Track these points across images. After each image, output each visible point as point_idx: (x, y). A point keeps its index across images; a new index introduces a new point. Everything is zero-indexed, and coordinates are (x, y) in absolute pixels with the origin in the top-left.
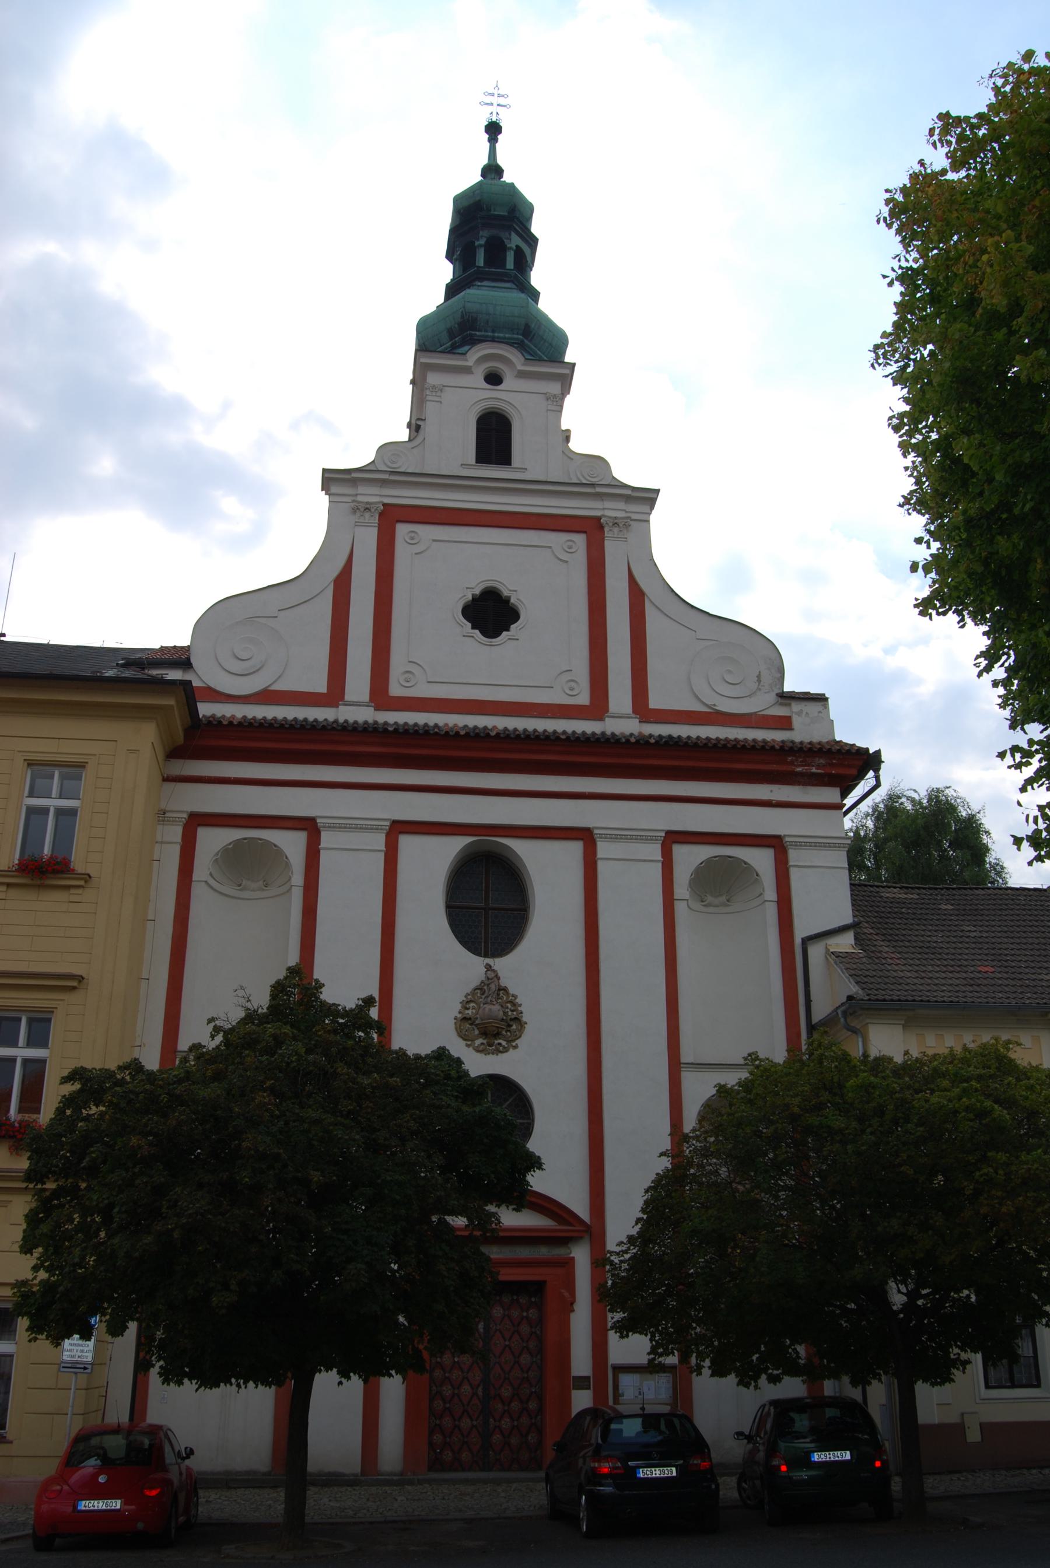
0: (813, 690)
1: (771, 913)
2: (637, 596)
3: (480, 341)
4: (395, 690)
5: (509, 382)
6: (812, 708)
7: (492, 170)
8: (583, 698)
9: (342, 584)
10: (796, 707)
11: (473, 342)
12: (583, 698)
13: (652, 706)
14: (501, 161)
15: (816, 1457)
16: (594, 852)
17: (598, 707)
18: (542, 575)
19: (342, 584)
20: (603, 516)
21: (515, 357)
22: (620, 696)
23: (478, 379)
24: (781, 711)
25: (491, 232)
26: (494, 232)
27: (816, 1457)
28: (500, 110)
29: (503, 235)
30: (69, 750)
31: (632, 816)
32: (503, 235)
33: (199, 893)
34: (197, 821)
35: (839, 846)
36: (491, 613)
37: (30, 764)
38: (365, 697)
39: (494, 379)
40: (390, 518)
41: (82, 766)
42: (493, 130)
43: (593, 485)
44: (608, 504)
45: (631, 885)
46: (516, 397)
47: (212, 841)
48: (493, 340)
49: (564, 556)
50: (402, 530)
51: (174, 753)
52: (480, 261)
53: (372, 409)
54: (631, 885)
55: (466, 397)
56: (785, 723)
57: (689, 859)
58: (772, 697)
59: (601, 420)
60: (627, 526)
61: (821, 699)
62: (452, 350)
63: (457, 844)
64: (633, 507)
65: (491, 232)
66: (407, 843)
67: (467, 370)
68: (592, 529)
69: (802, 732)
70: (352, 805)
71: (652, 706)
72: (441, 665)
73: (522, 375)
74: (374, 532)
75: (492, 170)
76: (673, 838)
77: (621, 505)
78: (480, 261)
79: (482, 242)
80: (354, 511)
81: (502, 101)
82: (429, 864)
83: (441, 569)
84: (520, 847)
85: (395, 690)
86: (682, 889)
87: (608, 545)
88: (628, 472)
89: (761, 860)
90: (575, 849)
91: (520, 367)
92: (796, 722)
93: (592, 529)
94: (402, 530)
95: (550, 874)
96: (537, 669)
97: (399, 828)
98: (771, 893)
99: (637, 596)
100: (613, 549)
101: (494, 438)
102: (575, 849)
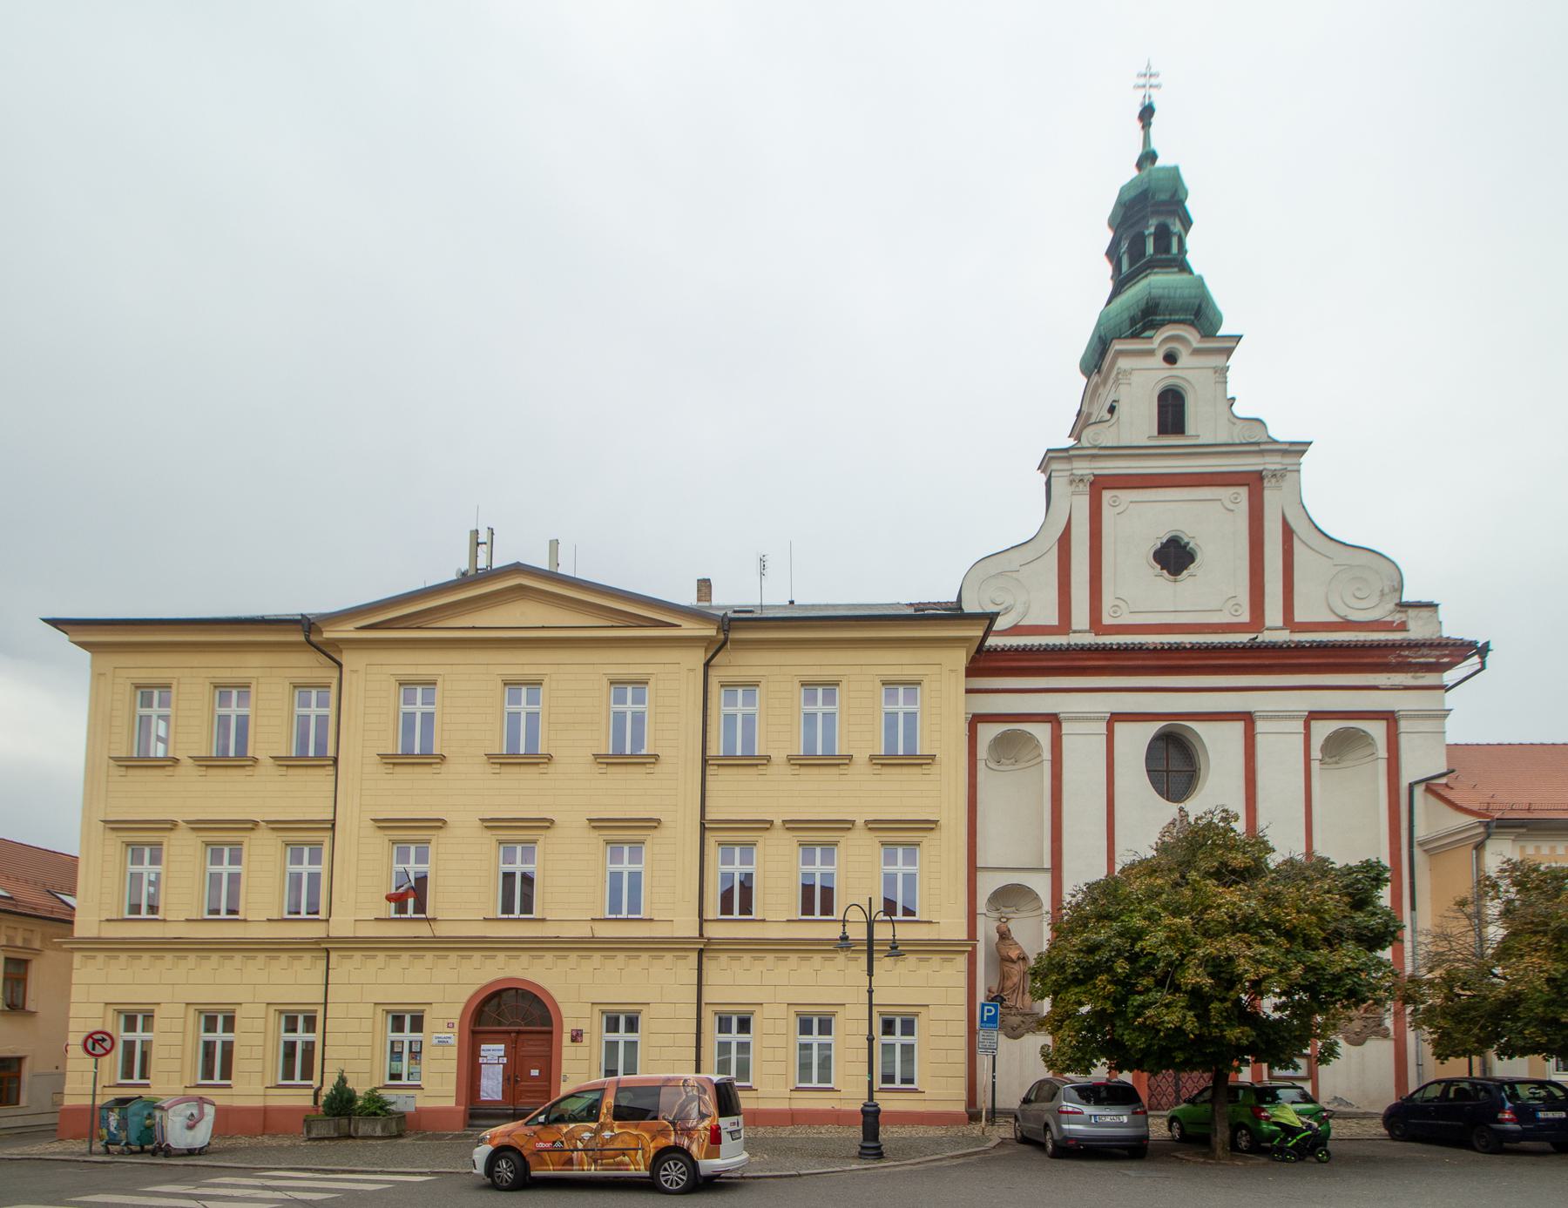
0: (1425, 599)
1: (1382, 766)
2: (1288, 533)
3: (1162, 324)
4: (1107, 620)
5: (1185, 359)
6: (1425, 613)
7: (1148, 158)
8: (1245, 617)
9: (1065, 542)
10: (1412, 612)
11: (1156, 326)
12: (1245, 617)
13: (1297, 619)
14: (1155, 145)
15: (1541, 1115)
16: (1253, 729)
17: (1065, 625)
18: (1214, 523)
19: (1065, 542)
20: (1257, 472)
21: (1192, 335)
22: (1273, 613)
23: (1158, 361)
24: (1398, 618)
25: (1149, 223)
26: (1162, 219)
27: (1541, 1115)
28: (1153, 92)
29: (1169, 221)
30: (827, 673)
31: (1281, 703)
32: (1169, 221)
33: (981, 766)
34: (976, 720)
35: (1297, 717)
36: (1174, 556)
37: (884, 683)
38: (1280, 623)
39: (1171, 358)
40: (1099, 485)
41: (837, 684)
42: (1147, 114)
43: (1258, 444)
44: (1268, 459)
45: (1281, 749)
46: (1191, 372)
47: (988, 733)
48: (1170, 322)
49: (1231, 506)
50: (1107, 495)
51: (971, 672)
52: (1150, 249)
53: (1048, 399)
54: (1281, 749)
55: (1140, 379)
56: (1402, 627)
57: (1322, 730)
58: (1391, 606)
59: (1260, 386)
60: (1283, 476)
61: (1432, 606)
62: (1135, 335)
63: (1155, 727)
64: (1288, 460)
65: (1149, 223)
66: (1119, 727)
67: (1151, 353)
68: (1254, 482)
69: (1418, 630)
70: (1083, 704)
71: (1297, 619)
72: (1140, 599)
73: (1197, 352)
74: (1086, 499)
75: (1148, 158)
76: (1315, 715)
77: (1277, 459)
78: (1150, 249)
79: (1152, 230)
80: (1071, 482)
81: (1153, 81)
82: (1135, 741)
83: (1138, 522)
84: (1196, 726)
85: (1107, 620)
86: (1316, 753)
87: (1267, 494)
88: (1280, 431)
89: (1377, 730)
90: (1239, 727)
91: (1195, 345)
92: (1411, 625)
93: (1254, 482)
94: (1107, 495)
95: (1220, 747)
96: (1211, 598)
97: (1116, 717)
98: (1382, 752)
99: (1288, 533)
100: (1273, 500)
101: (1172, 411)
102: (1239, 727)
